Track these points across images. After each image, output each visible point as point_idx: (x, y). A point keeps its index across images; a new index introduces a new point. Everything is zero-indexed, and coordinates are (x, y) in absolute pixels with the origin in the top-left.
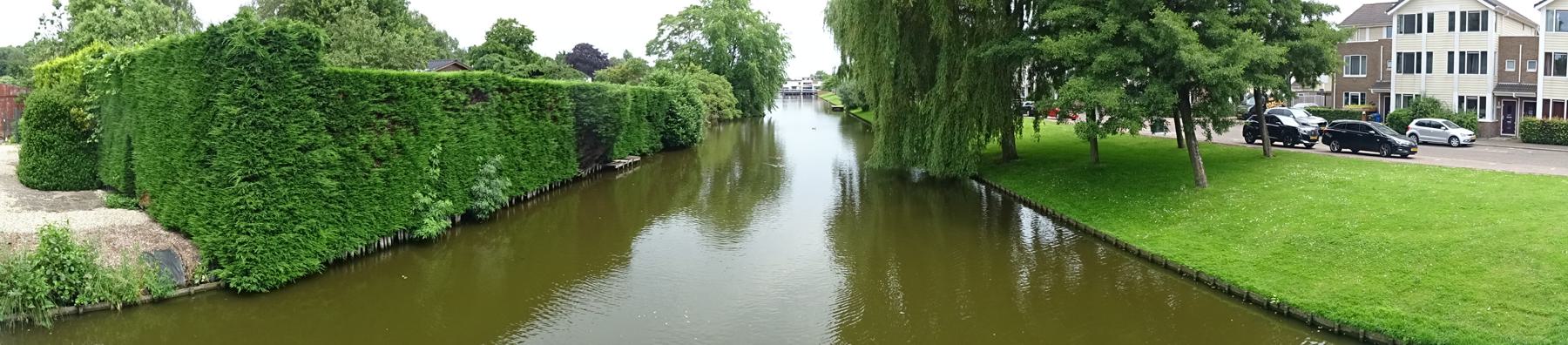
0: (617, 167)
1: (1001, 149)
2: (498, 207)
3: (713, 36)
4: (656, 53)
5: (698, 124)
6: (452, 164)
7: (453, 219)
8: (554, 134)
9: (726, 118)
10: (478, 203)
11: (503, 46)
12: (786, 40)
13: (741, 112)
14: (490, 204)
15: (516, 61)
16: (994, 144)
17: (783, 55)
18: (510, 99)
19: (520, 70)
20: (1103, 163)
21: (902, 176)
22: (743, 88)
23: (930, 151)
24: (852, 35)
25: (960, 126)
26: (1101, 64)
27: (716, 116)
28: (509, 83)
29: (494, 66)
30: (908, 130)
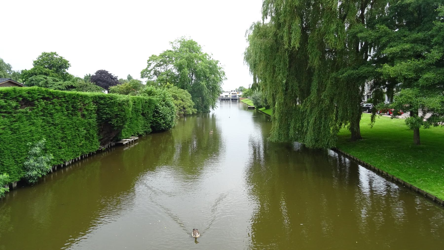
0: (124, 143)
1: (350, 133)
2: (45, 174)
3: (180, 68)
4: (146, 77)
5: (172, 117)
6: (7, 149)
7: (10, 185)
8: (83, 125)
9: (188, 113)
10: (29, 173)
11: (47, 69)
12: (222, 70)
13: (196, 110)
14: (38, 173)
15: (57, 79)
16: (345, 129)
17: (220, 78)
18: (53, 103)
19: (59, 85)
20: (423, 144)
21: (288, 147)
22: (198, 97)
23: (306, 133)
24: (261, 66)
25: (325, 118)
26: (427, 79)
27: (183, 112)
28: (51, 94)
29: (40, 83)
30: (293, 120)
